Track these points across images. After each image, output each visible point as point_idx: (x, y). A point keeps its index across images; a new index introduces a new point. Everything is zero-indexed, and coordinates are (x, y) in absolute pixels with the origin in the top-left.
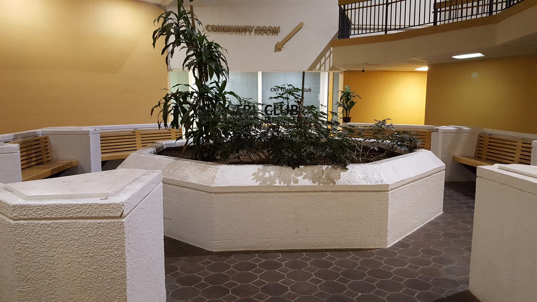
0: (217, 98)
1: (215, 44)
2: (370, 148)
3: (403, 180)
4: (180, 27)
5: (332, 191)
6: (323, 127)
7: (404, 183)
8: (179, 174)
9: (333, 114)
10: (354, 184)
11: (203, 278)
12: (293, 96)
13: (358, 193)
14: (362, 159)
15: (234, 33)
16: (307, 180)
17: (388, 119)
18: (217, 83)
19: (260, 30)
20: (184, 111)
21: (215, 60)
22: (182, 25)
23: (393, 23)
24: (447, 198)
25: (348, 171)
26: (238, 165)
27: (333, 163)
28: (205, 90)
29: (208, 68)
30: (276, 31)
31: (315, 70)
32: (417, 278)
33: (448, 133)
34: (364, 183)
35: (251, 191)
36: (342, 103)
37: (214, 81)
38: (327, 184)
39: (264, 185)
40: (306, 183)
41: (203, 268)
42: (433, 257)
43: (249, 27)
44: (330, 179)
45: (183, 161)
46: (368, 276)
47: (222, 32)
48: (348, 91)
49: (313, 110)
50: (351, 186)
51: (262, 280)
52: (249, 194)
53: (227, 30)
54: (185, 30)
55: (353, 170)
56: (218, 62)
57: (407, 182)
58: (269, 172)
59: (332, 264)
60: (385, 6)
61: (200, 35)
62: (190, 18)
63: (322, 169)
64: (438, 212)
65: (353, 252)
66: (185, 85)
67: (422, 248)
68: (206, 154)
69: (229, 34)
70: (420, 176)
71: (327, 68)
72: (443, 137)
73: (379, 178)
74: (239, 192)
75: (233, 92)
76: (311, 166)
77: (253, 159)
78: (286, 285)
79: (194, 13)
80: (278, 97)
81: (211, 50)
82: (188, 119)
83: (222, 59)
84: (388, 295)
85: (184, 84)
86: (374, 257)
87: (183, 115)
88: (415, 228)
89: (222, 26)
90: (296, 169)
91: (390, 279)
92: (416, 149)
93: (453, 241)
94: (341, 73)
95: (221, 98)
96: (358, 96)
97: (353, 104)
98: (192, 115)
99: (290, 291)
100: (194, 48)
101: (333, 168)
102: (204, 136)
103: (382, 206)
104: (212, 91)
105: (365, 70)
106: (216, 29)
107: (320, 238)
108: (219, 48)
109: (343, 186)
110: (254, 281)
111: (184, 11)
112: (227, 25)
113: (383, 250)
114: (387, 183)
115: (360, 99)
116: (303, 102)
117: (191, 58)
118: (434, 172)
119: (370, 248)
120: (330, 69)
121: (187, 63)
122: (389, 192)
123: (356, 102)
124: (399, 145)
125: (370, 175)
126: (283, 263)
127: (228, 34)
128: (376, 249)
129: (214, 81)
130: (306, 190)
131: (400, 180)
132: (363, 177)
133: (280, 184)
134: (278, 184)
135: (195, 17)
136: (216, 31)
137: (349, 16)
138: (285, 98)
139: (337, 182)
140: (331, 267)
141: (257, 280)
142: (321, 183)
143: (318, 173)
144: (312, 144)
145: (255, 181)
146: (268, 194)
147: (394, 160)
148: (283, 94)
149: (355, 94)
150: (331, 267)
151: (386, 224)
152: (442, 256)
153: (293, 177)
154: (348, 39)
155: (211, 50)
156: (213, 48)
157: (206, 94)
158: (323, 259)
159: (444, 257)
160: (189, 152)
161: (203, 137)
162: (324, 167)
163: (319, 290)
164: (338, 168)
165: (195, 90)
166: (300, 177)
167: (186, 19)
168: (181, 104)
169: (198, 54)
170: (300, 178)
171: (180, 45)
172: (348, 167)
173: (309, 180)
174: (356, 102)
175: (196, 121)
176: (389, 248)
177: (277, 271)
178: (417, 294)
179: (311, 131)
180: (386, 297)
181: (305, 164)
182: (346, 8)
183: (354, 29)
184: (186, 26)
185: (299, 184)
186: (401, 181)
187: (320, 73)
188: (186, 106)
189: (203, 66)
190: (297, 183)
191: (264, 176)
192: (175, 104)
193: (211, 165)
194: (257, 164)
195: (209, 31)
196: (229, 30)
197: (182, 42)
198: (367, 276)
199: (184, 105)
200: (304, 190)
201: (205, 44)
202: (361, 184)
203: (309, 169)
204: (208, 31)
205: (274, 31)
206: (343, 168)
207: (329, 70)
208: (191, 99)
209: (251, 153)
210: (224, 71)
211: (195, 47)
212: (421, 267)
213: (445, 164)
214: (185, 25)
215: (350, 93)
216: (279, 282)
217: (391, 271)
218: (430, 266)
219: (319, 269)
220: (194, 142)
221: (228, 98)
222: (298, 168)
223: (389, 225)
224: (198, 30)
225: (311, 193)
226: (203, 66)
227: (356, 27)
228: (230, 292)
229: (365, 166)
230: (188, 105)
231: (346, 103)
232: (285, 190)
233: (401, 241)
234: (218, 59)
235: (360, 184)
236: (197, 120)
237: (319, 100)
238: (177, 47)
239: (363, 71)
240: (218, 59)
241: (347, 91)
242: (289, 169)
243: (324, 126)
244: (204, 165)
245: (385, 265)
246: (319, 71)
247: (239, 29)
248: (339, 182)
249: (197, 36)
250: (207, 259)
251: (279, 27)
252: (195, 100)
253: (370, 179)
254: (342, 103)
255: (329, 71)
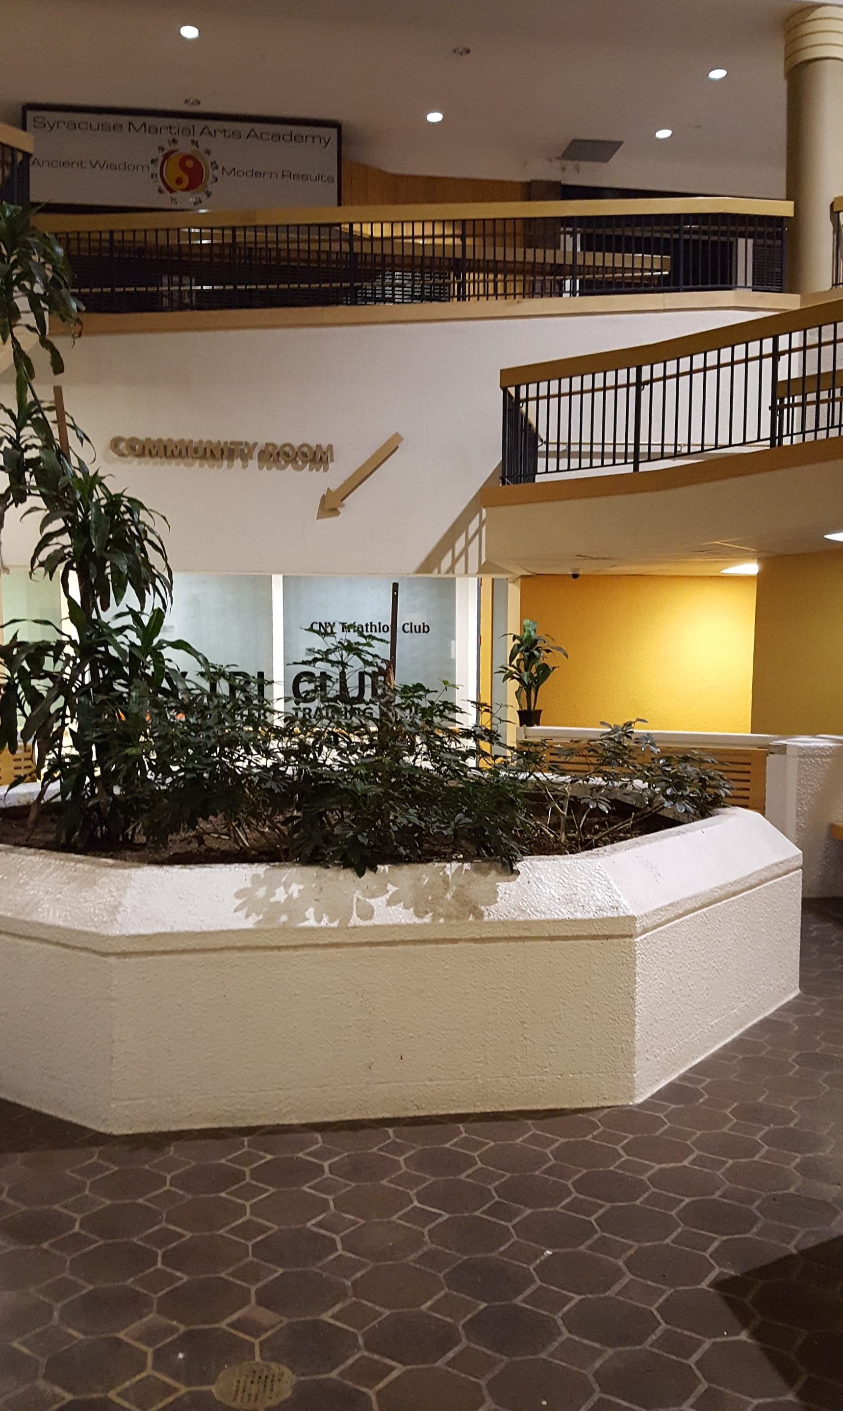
0: (134, 657)
1: (130, 500)
2: (587, 805)
3: (678, 903)
4: (25, 450)
5: (474, 940)
6: (449, 749)
7: (681, 912)
8: (10, 897)
9: (478, 709)
10: (535, 918)
11: (78, 1217)
12: (359, 656)
13: (549, 942)
14: (568, 838)
15: (198, 462)
16: (399, 908)
17: (638, 720)
18: (136, 616)
19: (275, 455)
20: (34, 697)
21: (128, 549)
22: (29, 442)
23: (656, 439)
24: (814, 948)
25: (518, 880)
26: (192, 866)
27: (479, 856)
28: (100, 635)
29: (108, 570)
30: (321, 459)
31: (439, 572)
32: (716, 1195)
33: (813, 756)
34: (564, 913)
35: (230, 944)
36: (513, 670)
37: (127, 610)
38: (457, 918)
39: (269, 927)
40: (397, 917)
41: (80, 1188)
42: (766, 1129)
43: (241, 443)
44: (467, 905)
45: (22, 856)
46: (575, 1194)
47: (161, 457)
48: (533, 633)
49: (420, 697)
50: (529, 924)
51: (260, 1220)
52: (226, 954)
53: (176, 452)
54: (38, 459)
55: (534, 876)
56: (137, 552)
57: (688, 907)
58: (287, 886)
59: (470, 1162)
60: (633, 390)
61: (85, 473)
62: (54, 422)
63: (444, 873)
64: (786, 991)
65: (533, 1121)
66: (36, 621)
67: (736, 1104)
68: (101, 828)
69: (182, 466)
70: (728, 889)
71: (474, 566)
72: (799, 769)
73: (606, 897)
74: (194, 951)
75: (185, 640)
76: (412, 865)
77: (244, 844)
78: (329, 1234)
79: (66, 410)
80: (315, 660)
81: (119, 516)
82: (44, 724)
83: (151, 543)
84: (631, 1252)
85: (35, 618)
86: (595, 1133)
87: (33, 709)
88: (716, 1043)
89: (160, 441)
90: (368, 874)
91: (638, 1202)
92: (718, 807)
93: (825, 1081)
94: (514, 582)
95: (149, 658)
96: (560, 649)
97: (545, 671)
98: (58, 710)
99: (340, 1251)
100: (66, 513)
101: (477, 869)
102: (98, 772)
103: (618, 981)
104: (119, 638)
105: (581, 572)
106: (141, 451)
107: (439, 1082)
108: (142, 512)
109: (504, 923)
110: (233, 1225)
111: (37, 402)
112: (176, 438)
113: (622, 1112)
114: (631, 912)
115: (567, 657)
116: (394, 672)
117: (55, 540)
118: (770, 874)
119: (585, 1105)
120: (483, 569)
121: (43, 556)
122: (638, 939)
123: (554, 668)
124: (667, 797)
125: (583, 890)
126: (326, 1165)
127: (178, 464)
128: (603, 1108)
129: (127, 610)
130: (397, 938)
131: (668, 903)
132: (563, 896)
133: (319, 921)
134: (312, 923)
135: (68, 420)
136: (141, 455)
137: (532, 418)
138: (338, 662)
139: (486, 913)
140: (470, 1171)
141: (244, 1219)
142: (440, 915)
143: (431, 886)
144: (416, 799)
145: (241, 914)
146: (284, 953)
147: (653, 844)
148: (329, 652)
149: (552, 644)
150: (470, 1171)
151: (628, 1034)
152: (792, 1125)
153: (358, 900)
154: (530, 484)
155: (119, 516)
156: (124, 513)
157: (102, 649)
158: (447, 1145)
159: (797, 1127)
160: (53, 821)
161: (93, 778)
162: (451, 868)
163: (429, 1246)
164: (490, 869)
165: (69, 637)
166: (380, 898)
167: (42, 427)
168: (25, 677)
169: (80, 531)
170: (378, 903)
171: (23, 500)
172: (518, 866)
173: (406, 907)
174: (554, 668)
175: (71, 730)
176: (639, 1106)
177: (308, 1190)
178: (716, 1244)
179: (414, 761)
180: (624, 1257)
181: (396, 860)
182: (523, 396)
183: (547, 454)
184: (41, 449)
185: (376, 921)
186: (671, 905)
187: (453, 580)
188: (41, 685)
189: (91, 565)
190: (371, 918)
191: (272, 900)
192: (8, 678)
193: (108, 869)
194: (251, 860)
195: (122, 455)
196: (180, 452)
197: (30, 494)
198: (573, 1196)
199: (34, 682)
200: (390, 939)
201: (99, 500)
202: (556, 917)
203: (406, 872)
204: (116, 456)
205: (318, 458)
206: (506, 871)
207: (478, 573)
208: (55, 662)
209: (239, 825)
210: (157, 580)
211: (66, 510)
212: (731, 1162)
213: (801, 852)
214: (39, 442)
215: (536, 641)
216: (309, 1224)
217: (644, 1177)
218: (756, 1158)
219: (433, 1179)
220: (63, 792)
221: (170, 660)
222: (372, 873)
223: (638, 1035)
224: (79, 460)
225: (411, 948)
226: (91, 565)
227: (553, 448)
228: (160, 1260)
229: (568, 863)
230: (48, 682)
231: (526, 670)
232: (335, 941)
233: (677, 1082)
234: (137, 545)
235: (553, 917)
236: (74, 727)
237: (452, 657)
238: (16, 506)
239: (575, 576)
240: (137, 545)
241: (530, 636)
242: (348, 876)
243: (453, 743)
244: (87, 867)
245: (625, 1157)
246: (450, 575)
247: (212, 451)
248: (495, 912)
249: (75, 476)
250: (95, 1158)
251: (330, 447)
252: (66, 664)
253: (582, 900)
254: (513, 670)
255: (480, 576)
